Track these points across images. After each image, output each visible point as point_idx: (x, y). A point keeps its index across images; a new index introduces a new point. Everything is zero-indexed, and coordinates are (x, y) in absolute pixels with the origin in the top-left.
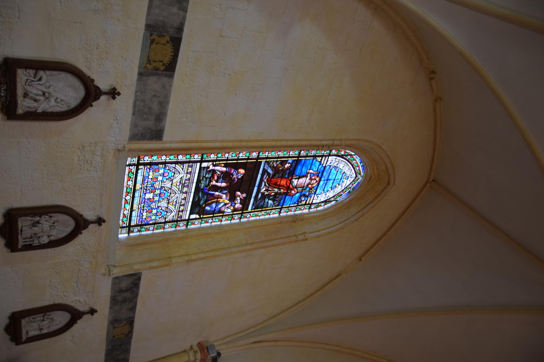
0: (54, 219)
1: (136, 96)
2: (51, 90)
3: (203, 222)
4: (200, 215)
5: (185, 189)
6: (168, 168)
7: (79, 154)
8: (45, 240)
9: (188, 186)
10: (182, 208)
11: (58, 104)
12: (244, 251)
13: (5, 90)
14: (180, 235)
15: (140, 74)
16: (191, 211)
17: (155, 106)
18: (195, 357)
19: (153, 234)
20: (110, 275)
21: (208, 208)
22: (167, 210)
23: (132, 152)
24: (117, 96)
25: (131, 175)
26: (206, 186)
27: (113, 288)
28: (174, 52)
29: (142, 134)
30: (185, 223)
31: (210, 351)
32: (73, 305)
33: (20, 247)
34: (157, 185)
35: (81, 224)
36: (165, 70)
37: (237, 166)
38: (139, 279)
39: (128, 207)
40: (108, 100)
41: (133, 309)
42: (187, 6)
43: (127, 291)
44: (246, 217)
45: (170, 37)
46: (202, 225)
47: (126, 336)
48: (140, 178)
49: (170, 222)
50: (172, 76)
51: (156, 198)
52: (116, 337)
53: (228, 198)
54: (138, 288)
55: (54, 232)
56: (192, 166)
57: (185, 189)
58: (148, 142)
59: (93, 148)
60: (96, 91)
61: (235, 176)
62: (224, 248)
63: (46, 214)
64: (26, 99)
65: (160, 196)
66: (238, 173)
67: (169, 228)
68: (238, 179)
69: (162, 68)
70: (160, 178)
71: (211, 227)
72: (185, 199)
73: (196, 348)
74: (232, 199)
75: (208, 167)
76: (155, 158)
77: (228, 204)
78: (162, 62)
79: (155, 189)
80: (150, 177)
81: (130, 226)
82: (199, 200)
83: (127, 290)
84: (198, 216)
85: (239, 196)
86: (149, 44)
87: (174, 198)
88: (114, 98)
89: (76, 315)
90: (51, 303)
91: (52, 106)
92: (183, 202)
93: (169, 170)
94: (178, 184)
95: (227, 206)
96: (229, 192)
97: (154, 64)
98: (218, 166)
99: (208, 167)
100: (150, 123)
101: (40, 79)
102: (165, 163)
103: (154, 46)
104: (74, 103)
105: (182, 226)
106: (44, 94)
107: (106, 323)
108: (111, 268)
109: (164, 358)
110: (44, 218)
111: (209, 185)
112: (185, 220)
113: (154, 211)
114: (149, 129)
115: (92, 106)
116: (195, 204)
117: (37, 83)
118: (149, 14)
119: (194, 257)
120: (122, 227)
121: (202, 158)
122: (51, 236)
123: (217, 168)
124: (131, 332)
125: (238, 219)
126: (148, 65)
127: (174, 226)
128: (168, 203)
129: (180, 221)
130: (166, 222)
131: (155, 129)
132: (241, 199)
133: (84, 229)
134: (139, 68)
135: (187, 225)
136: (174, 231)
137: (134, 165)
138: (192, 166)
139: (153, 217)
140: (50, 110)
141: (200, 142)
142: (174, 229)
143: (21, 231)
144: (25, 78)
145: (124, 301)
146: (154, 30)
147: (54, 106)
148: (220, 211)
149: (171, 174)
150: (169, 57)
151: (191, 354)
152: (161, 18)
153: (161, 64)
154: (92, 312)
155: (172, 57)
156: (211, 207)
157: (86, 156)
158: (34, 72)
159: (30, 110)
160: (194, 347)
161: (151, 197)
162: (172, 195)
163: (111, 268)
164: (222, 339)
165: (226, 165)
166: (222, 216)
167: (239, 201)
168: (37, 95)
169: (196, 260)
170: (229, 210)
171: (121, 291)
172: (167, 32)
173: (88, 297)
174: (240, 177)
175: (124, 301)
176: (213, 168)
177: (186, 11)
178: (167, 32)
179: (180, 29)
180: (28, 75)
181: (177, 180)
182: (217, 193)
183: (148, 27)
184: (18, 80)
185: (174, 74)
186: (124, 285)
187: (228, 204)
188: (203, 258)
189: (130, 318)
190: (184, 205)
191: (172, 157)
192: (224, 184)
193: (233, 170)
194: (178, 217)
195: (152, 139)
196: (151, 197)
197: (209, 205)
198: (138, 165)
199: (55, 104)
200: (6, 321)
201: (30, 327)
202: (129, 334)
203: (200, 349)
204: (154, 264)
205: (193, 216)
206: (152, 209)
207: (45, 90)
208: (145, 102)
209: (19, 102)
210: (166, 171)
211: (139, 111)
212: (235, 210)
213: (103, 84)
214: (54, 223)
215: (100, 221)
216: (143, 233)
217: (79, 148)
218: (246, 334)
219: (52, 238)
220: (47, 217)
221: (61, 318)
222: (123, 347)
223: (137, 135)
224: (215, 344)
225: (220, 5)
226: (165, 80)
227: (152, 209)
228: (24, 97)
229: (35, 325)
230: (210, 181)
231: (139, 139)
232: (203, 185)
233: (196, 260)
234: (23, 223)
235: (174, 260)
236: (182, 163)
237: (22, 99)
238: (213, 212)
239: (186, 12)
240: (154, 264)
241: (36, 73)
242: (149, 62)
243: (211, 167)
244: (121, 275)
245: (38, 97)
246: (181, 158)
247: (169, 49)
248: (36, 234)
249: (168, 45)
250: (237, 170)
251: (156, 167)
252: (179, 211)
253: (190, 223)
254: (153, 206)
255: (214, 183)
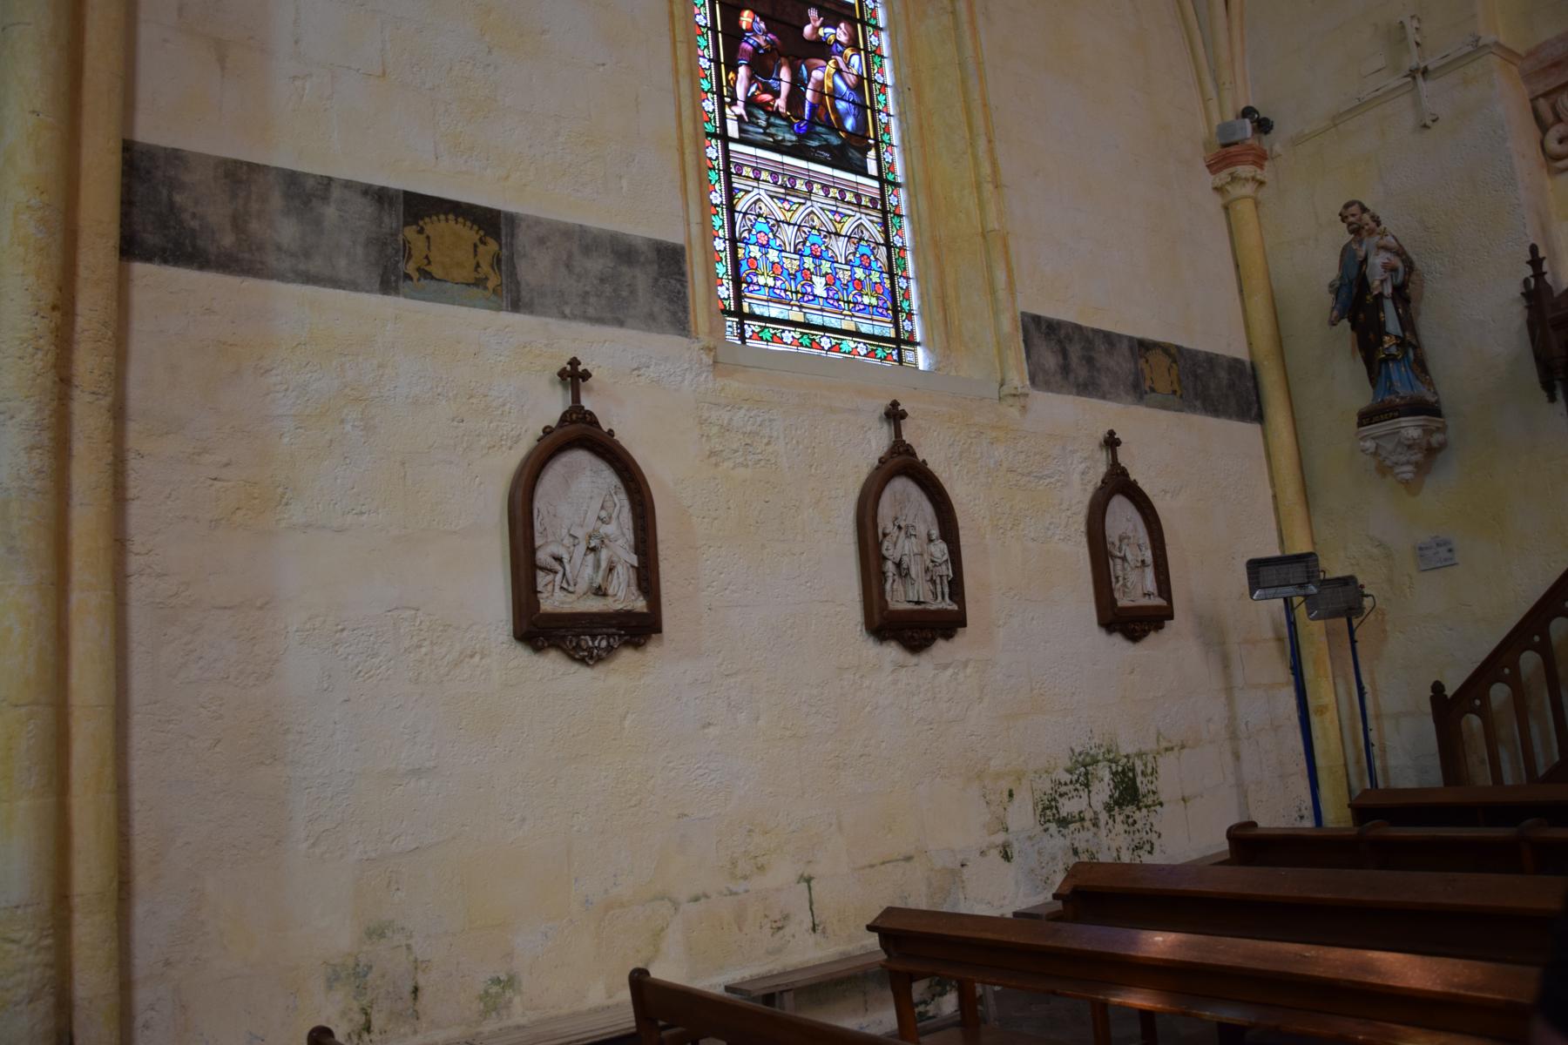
0: (890, 528)
1: (574, 317)
2: (580, 533)
3: (886, 138)
4: (869, 148)
5: (800, 185)
6: (746, 234)
7: (729, 464)
8: (940, 549)
9: (793, 179)
10: (849, 197)
11: (614, 515)
12: (972, 22)
13: (594, 637)
14: (923, 205)
15: (516, 306)
16: (857, 173)
17: (597, 265)
18: (1246, 179)
19: (917, 279)
20: (1026, 395)
21: (849, 123)
22: (855, 239)
23: (717, 330)
24: (580, 368)
25: (767, 335)
26: (791, 125)
27: (1059, 390)
28: (446, 214)
29: (671, 301)
30: (889, 189)
31: (1236, 138)
32: (1090, 490)
33: (955, 607)
34: (791, 264)
35: (901, 463)
36: (498, 238)
37: (733, 35)
38: (1037, 319)
39: (848, 344)
40: (590, 390)
41: (1110, 339)
42: (314, 176)
43: (1066, 353)
44: (873, 10)
45: (406, 224)
46: (895, 141)
47: (1175, 361)
48: (775, 311)
49: (886, 232)
50: (512, 219)
51: (826, 266)
52: (1176, 387)
53: (822, 63)
54: (1060, 324)
55: (922, 530)
56: (740, 166)
57: (800, 185)
58: (689, 285)
59: (715, 430)
60: (572, 422)
61: (761, 40)
62: (964, 81)
63: (879, 545)
64: (610, 591)
65: (820, 257)
66: (751, 30)
67: (904, 235)
68: (769, 30)
69: (493, 245)
70: (773, 255)
71: (902, 116)
72: (825, 188)
73: (1224, 175)
74: (823, 49)
75: (740, 118)
76: (721, 269)
77: (836, 63)
78: (475, 246)
79: (802, 269)
80: (771, 282)
81: (898, 341)
82: (827, 147)
83: (1065, 354)
84: (872, 154)
85: (816, 29)
86: (433, 283)
87: (824, 220)
88: (586, 375)
89: (1118, 483)
90: (1084, 540)
91: (620, 530)
92: (833, 192)
93: (750, 231)
94: (787, 206)
95: (842, 66)
96: (805, 58)
97: (485, 268)
98: (734, 89)
99: (740, 118)
100: (642, 279)
101: (559, 560)
102: (733, 241)
103: (435, 270)
104: (607, 478)
105: (899, 199)
106: (593, 550)
107: (1141, 411)
108: (1006, 390)
109: (1237, 266)
110: (888, 549)
111: (786, 119)
112: (882, 189)
113: (860, 274)
114: (651, 281)
115: (611, 432)
116: (840, 159)
117: (568, 567)
118: (353, 286)
119: (986, 169)
120: (900, 360)
121: (714, 135)
122: (929, 535)
123: (740, 92)
124: (1166, 349)
125: (877, 36)
126: (490, 285)
127: (896, 220)
128: (838, 234)
129: (884, 205)
130: (888, 244)
131: (656, 267)
132: (824, 25)
133: (914, 454)
134: (499, 309)
135: (895, 185)
136: (912, 222)
137: (741, 325)
138: (740, 166)
139: (875, 277)
140: (630, 536)
141: (681, 140)
142: (905, 222)
143: (918, 603)
144: (559, 594)
145: (1090, 361)
146: (393, 271)
147: (620, 525)
148: (858, 88)
149: (761, 226)
150: (460, 226)
151: (1237, 191)
152: (360, 251)
153: (481, 248)
154: (1111, 442)
155: (460, 220)
156: (848, 114)
157: (735, 447)
158: (540, 574)
159: (633, 581)
160: (1218, 183)
161: (823, 280)
162: (817, 223)
163: (1006, 390)
164: (1205, 101)
165: (733, 67)
166: (871, 81)
167: (829, 30)
168: (597, 566)
169: (994, 164)
170: (855, 60)
171: (1065, 369)
172: (394, 235)
173: (1073, 452)
174: (762, 25)
175: (1090, 361)
176: (740, 104)
177: (328, 182)
178: (394, 235)
179: (381, 196)
180: (550, 587)
181: (776, 209)
182: (809, 95)
183: (388, 285)
184: (567, 609)
185: (507, 214)
186: (1051, 361)
187: (836, 63)
188: (990, 141)
189: (1131, 348)
190: (842, 191)
191: (717, 222)
192: (785, 74)
193: (744, 45)
194: (875, 208)
195: (683, 274)
196: (823, 280)
197: (841, 119)
198: (739, 314)
199: (614, 522)
200: (1117, 640)
201: (1136, 588)
202: (1173, 353)
203: (1226, 166)
204: (1001, 277)
205: (872, 168)
206: (853, 280)
207: (582, 548)
208: (587, 293)
209: (618, 606)
210: (754, 239)
211: (614, 312)
212: (853, 43)
213: (552, 406)
214: (900, 528)
215: (895, 415)
216: (915, 307)
217: (716, 465)
218: (1200, 27)
219: (935, 533)
220: (886, 544)
221: (1122, 518)
222: (1200, 371)
223: (674, 314)
224: (1216, 121)
225: (295, 78)
226: (523, 239)
227: (853, 280)
228: (605, 595)
229: (1133, 577)
230: (777, 114)
231: (685, 310)
232: (788, 136)
233: (994, 164)
234: (900, 598)
235: (993, 224)
236: (731, 192)
237: (610, 600)
238: (861, 107)
239: (330, 179)
240: (1001, 277)
241: (542, 569)
242: (479, 283)
243: (739, 109)
244: (1025, 365)
245: (604, 565)
246: (717, 198)
247: (440, 227)
248: (927, 570)
249: (429, 229)
250: (743, 32)
251: (744, 267)
252: (859, 205)
253: (890, 177)
254: (844, 276)
255: (781, 103)
